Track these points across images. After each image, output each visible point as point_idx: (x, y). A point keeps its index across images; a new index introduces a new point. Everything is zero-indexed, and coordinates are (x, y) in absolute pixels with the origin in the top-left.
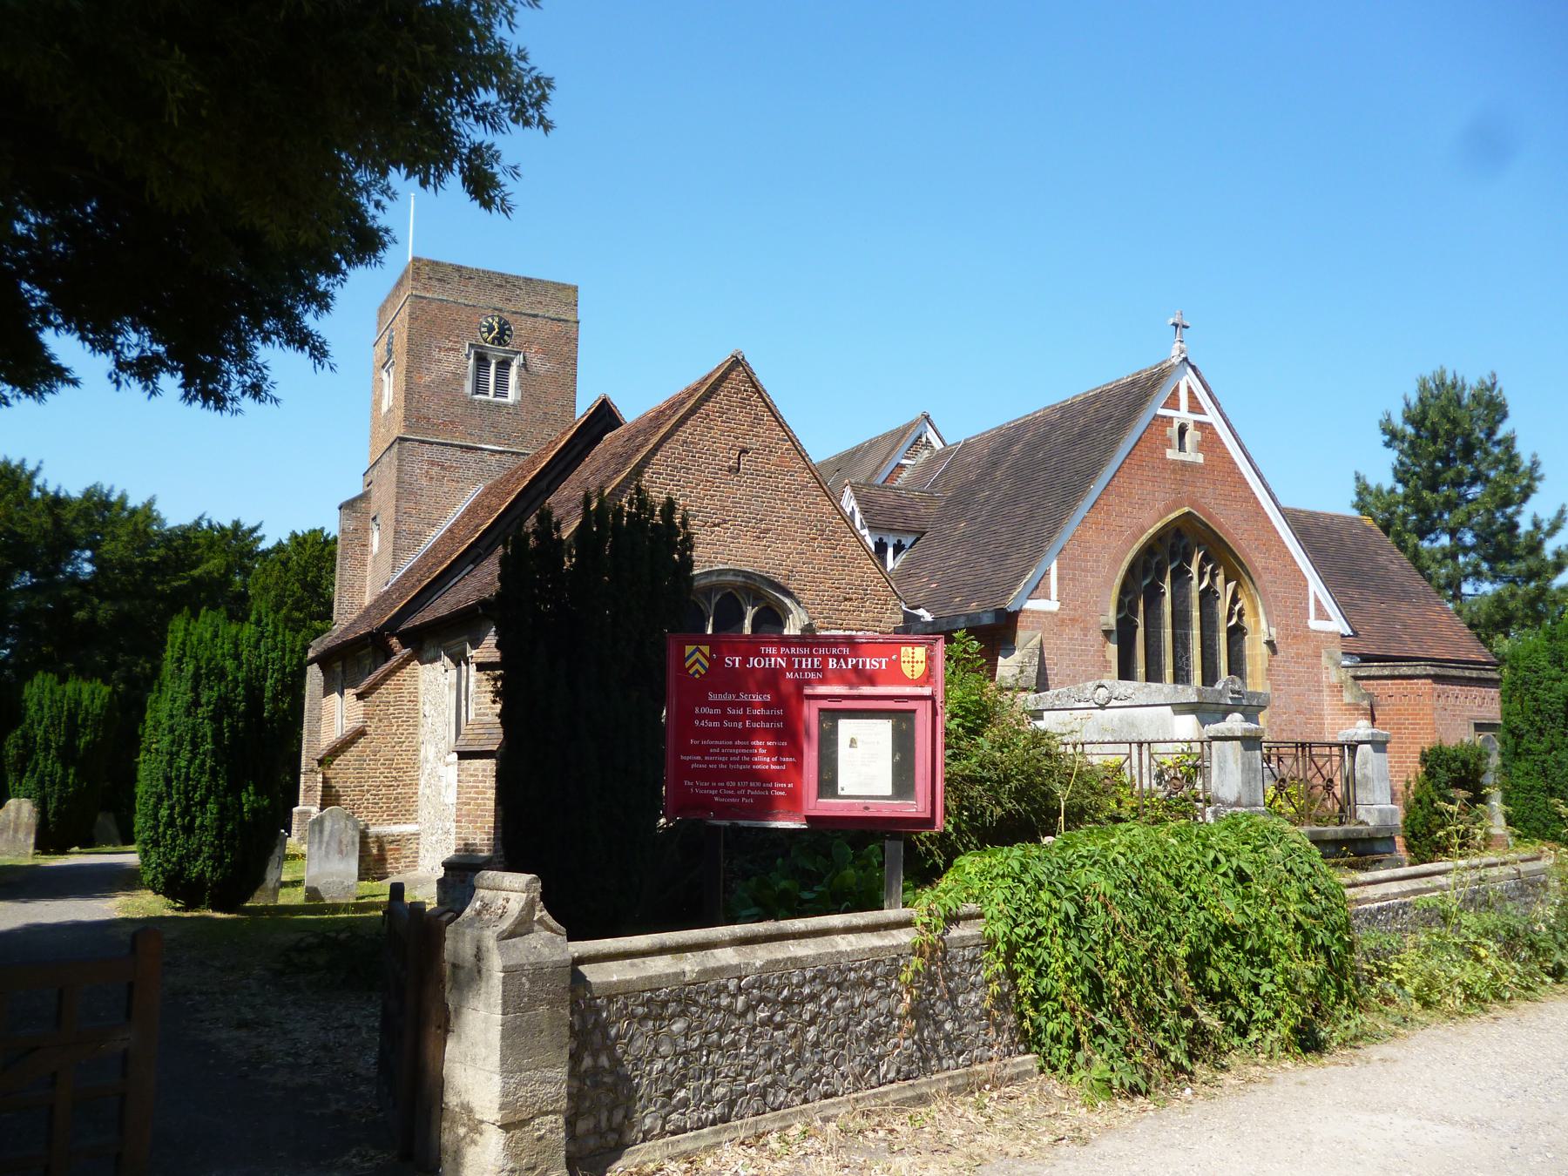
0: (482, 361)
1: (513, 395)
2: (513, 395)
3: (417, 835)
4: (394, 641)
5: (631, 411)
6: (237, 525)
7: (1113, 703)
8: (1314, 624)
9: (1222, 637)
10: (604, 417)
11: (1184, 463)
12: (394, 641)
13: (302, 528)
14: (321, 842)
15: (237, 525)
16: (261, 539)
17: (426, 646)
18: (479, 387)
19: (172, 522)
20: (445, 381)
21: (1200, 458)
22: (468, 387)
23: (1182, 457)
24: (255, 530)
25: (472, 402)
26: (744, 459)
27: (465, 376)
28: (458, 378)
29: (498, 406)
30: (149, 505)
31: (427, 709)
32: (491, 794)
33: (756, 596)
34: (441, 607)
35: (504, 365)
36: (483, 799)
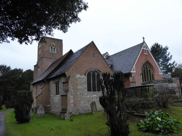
0: (52, 48)
1: (55, 52)
2: (55, 52)
3: (50, 107)
4: (45, 80)
5: (74, 51)
6: (75, 18)
7: (158, 83)
8: (160, 74)
9: (151, 75)
10: (71, 52)
11: (146, 55)
12: (45, 80)
13: (28, 69)
15: (75, 18)
16: (23, 71)
19: (12, 69)
21: (147, 54)
22: (50, 51)
23: (146, 54)
24: (22, 70)
27: (50, 50)
29: (54, 53)
30: (9, 67)
31: (51, 90)
32: (101, 106)
33: (97, 72)
34: (54, 75)
35: (54, 48)
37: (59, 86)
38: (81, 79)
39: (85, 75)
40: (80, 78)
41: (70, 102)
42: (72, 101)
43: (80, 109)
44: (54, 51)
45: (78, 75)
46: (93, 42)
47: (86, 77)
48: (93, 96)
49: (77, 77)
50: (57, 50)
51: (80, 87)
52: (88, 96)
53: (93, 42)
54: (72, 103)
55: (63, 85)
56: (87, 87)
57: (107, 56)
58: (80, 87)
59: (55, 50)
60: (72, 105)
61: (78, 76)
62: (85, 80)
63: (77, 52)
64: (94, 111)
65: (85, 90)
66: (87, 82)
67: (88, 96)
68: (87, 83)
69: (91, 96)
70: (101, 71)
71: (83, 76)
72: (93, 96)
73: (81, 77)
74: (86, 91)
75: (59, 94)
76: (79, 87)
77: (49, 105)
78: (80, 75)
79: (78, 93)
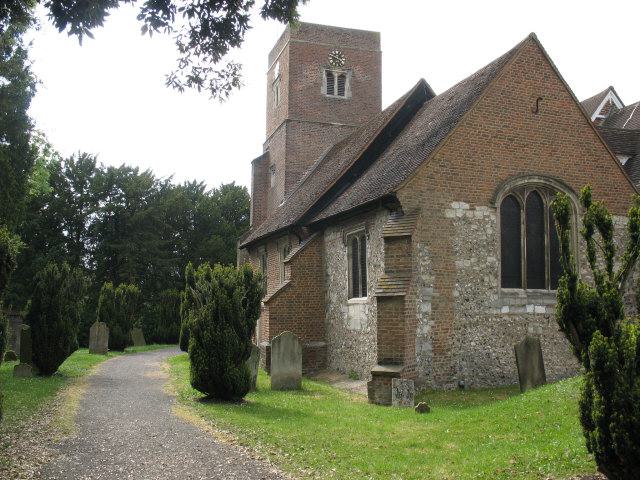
0: (329, 75)
1: (347, 94)
3: (325, 348)
5: (439, 88)
13: (227, 182)
14: (279, 354)
16: (204, 187)
17: (326, 232)
18: (330, 91)
20: (309, 88)
22: (324, 90)
25: (326, 99)
26: (540, 103)
28: (318, 85)
34: (332, 211)
35: (342, 77)
36: (396, 328)
37: (368, 255)
38: (474, 227)
39: (492, 203)
40: (464, 218)
41: (419, 330)
42: (426, 329)
43: (461, 369)
44: (341, 91)
45: (455, 205)
46: (532, 39)
47: (495, 218)
48: (530, 309)
49: (450, 214)
50: (355, 84)
51: (467, 264)
52: (505, 310)
53: (532, 39)
54: (425, 339)
55: (386, 250)
56: (498, 265)
57: (610, 106)
58: (467, 264)
59: (347, 85)
60: (428, 346)
61: (458, 209)
62: (490, 231)
63: (451, 95)
64: (532, 381)
65: (492, 277)
66: (499, 240)
67: (505, 310)
68: (498, 245)
69: (521, 310)
70: (571, 185)
71: (482, 211)
72: (530, 309)
73: (469, 214)
74: (496, 283)
75: (365, 295)
76: (461, 263)
77: (323, 344)
78: (467, 206)
79: (456, 294)
